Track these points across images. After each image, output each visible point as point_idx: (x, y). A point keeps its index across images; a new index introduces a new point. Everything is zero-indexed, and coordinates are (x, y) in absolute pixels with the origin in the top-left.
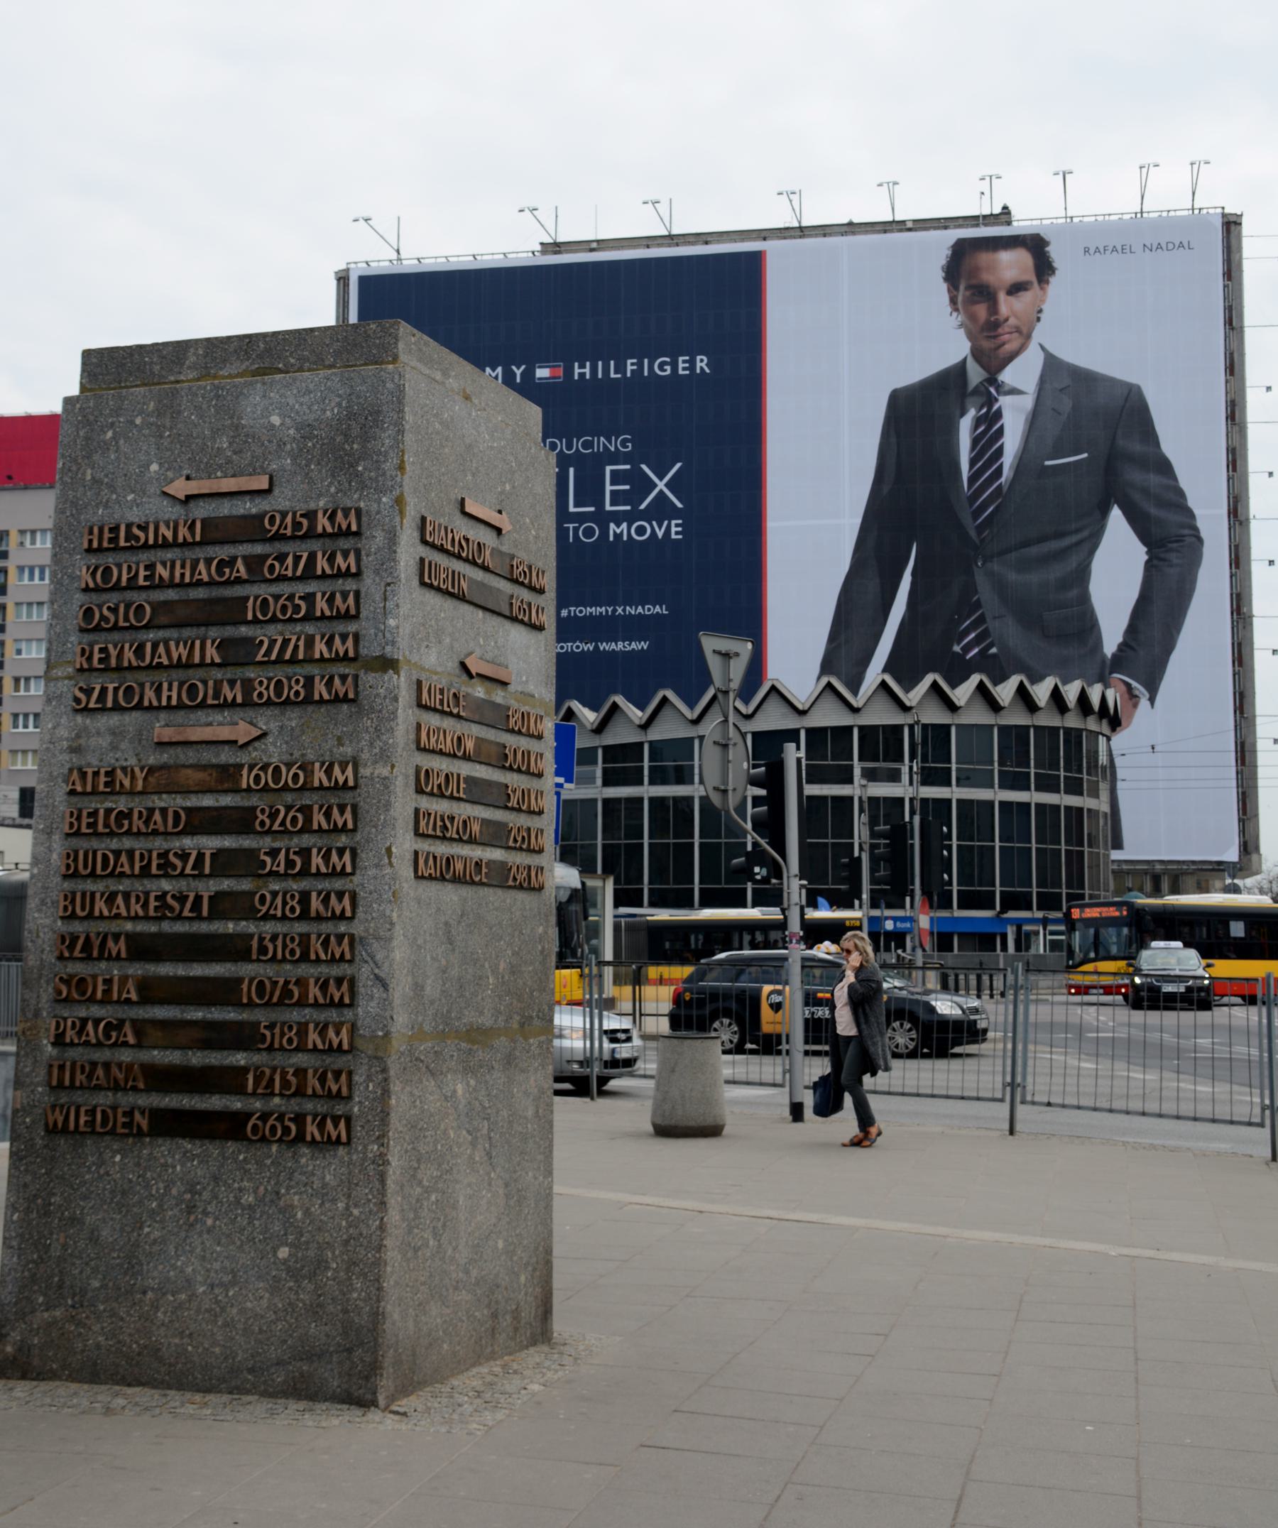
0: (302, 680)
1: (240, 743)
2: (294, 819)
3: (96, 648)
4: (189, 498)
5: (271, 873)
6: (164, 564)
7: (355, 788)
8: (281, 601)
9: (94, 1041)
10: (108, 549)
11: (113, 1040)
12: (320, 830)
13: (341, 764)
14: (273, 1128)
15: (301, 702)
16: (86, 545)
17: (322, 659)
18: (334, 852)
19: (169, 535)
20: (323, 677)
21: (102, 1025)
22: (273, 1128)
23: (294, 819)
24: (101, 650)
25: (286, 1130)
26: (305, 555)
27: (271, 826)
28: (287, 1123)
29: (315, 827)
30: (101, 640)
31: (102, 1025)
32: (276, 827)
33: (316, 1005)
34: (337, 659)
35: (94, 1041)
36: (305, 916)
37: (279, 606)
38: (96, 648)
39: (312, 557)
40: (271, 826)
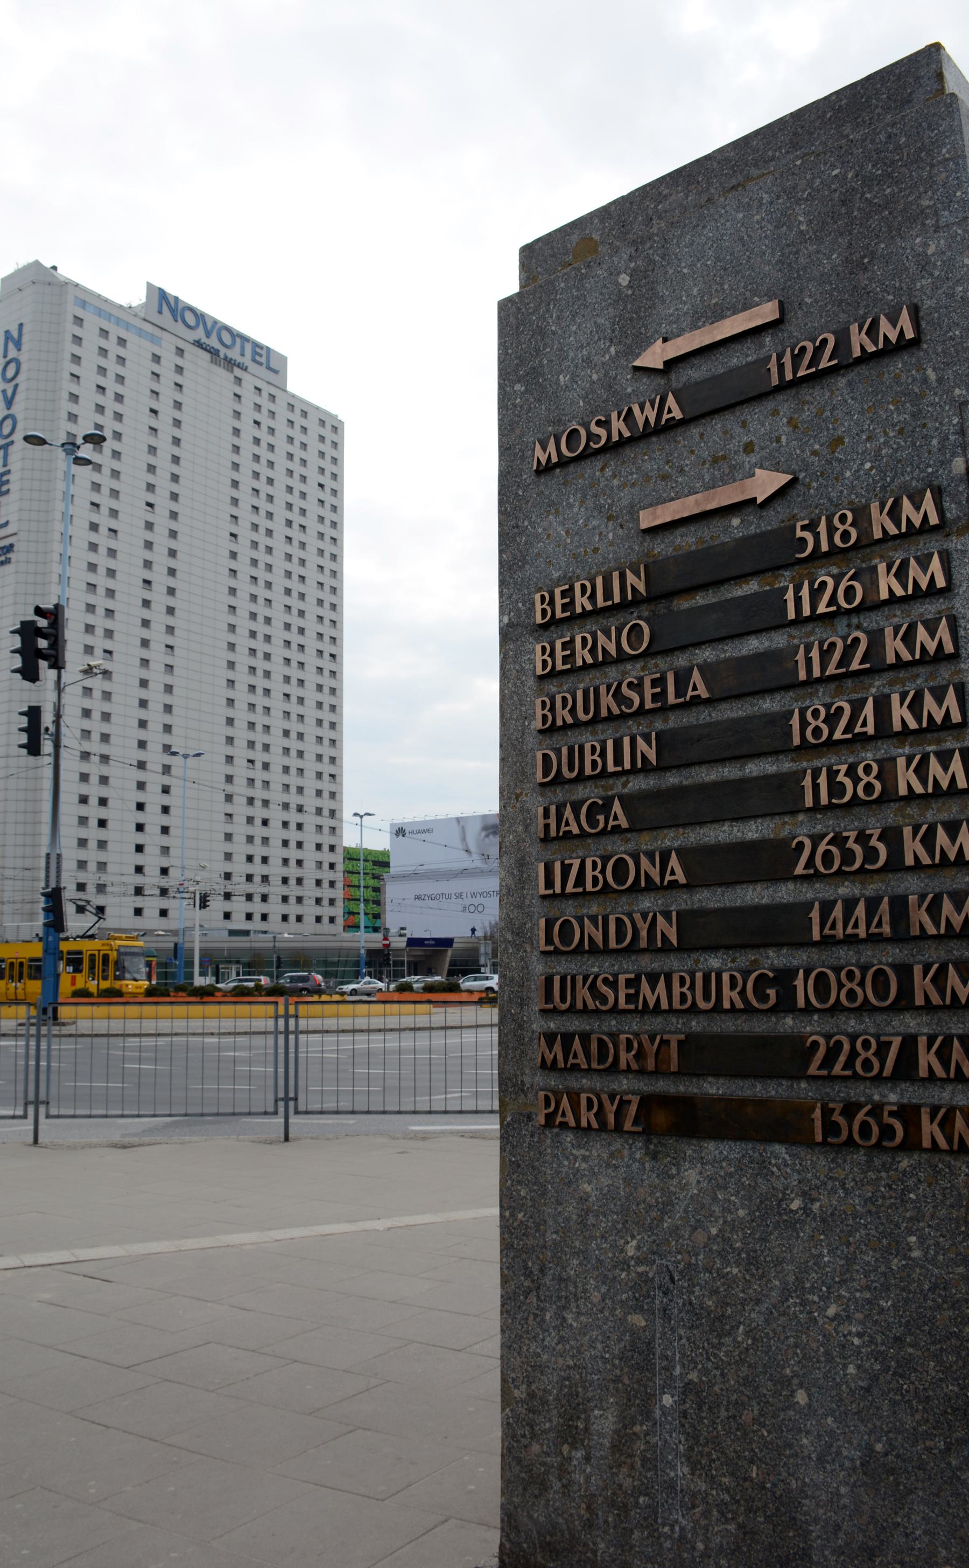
0: (850, 516)
1: (759, 501)
2: (850, 591)
3: (557, 592)
4: (671, 364)
5: (816, 555)
6: (650, 856)
7: (955, 656)
8: (860, 1116)
9: (576, 831)
10: (563, 672)
11: (601, 825)
12: (929, 1007)
13: (926, 624)
14: (865, 1126)
15: (878, 801)
16: (538, 724)
17: (893, 599)
18: (940, 831)
19: (655, 874)
20: (922, 897)
21: (584, 810)
22: (865, 1129)
23: (850, 591)
24: (565, 646)
25: (888, 1132)
26: (897, 1042)
27: (831, 733)
28: (887, 1119)
29: (919, 1001)
30: (563, 743)
31: (584, 810)
32: (838, 735)
33: (929, 1007)
34: (918, 595)
35: (576, 831)
36: (901, 935)
37: (856, 1127)
38: (557, 592)
39: (909, 1042)
40: (831, 733)
